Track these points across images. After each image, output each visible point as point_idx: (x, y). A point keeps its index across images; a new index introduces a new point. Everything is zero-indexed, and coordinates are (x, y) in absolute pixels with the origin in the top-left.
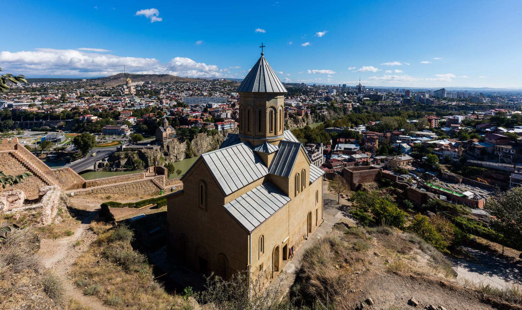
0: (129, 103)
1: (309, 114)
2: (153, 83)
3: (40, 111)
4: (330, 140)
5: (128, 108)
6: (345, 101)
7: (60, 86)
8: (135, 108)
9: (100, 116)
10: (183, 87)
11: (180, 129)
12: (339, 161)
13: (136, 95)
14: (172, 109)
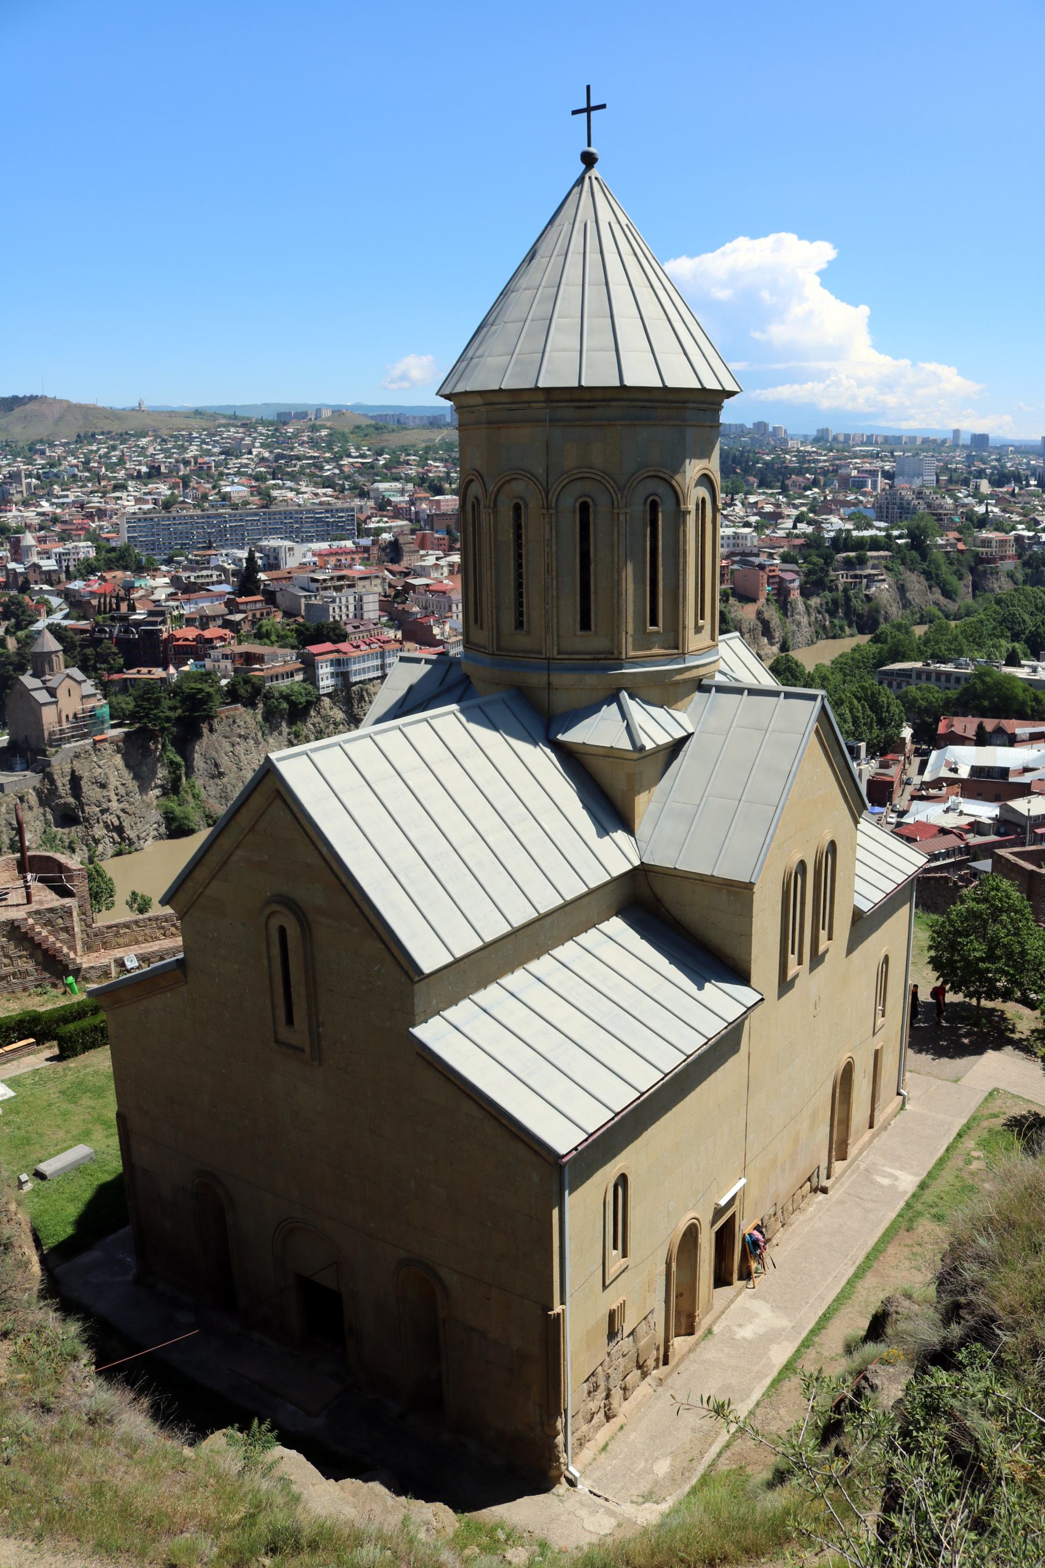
1: (795, 595)
4: (899, 726)
6: (982, 522)
10: (121, 461)
11: (125, 686)
12: (944, 831)
14: (77, 585)
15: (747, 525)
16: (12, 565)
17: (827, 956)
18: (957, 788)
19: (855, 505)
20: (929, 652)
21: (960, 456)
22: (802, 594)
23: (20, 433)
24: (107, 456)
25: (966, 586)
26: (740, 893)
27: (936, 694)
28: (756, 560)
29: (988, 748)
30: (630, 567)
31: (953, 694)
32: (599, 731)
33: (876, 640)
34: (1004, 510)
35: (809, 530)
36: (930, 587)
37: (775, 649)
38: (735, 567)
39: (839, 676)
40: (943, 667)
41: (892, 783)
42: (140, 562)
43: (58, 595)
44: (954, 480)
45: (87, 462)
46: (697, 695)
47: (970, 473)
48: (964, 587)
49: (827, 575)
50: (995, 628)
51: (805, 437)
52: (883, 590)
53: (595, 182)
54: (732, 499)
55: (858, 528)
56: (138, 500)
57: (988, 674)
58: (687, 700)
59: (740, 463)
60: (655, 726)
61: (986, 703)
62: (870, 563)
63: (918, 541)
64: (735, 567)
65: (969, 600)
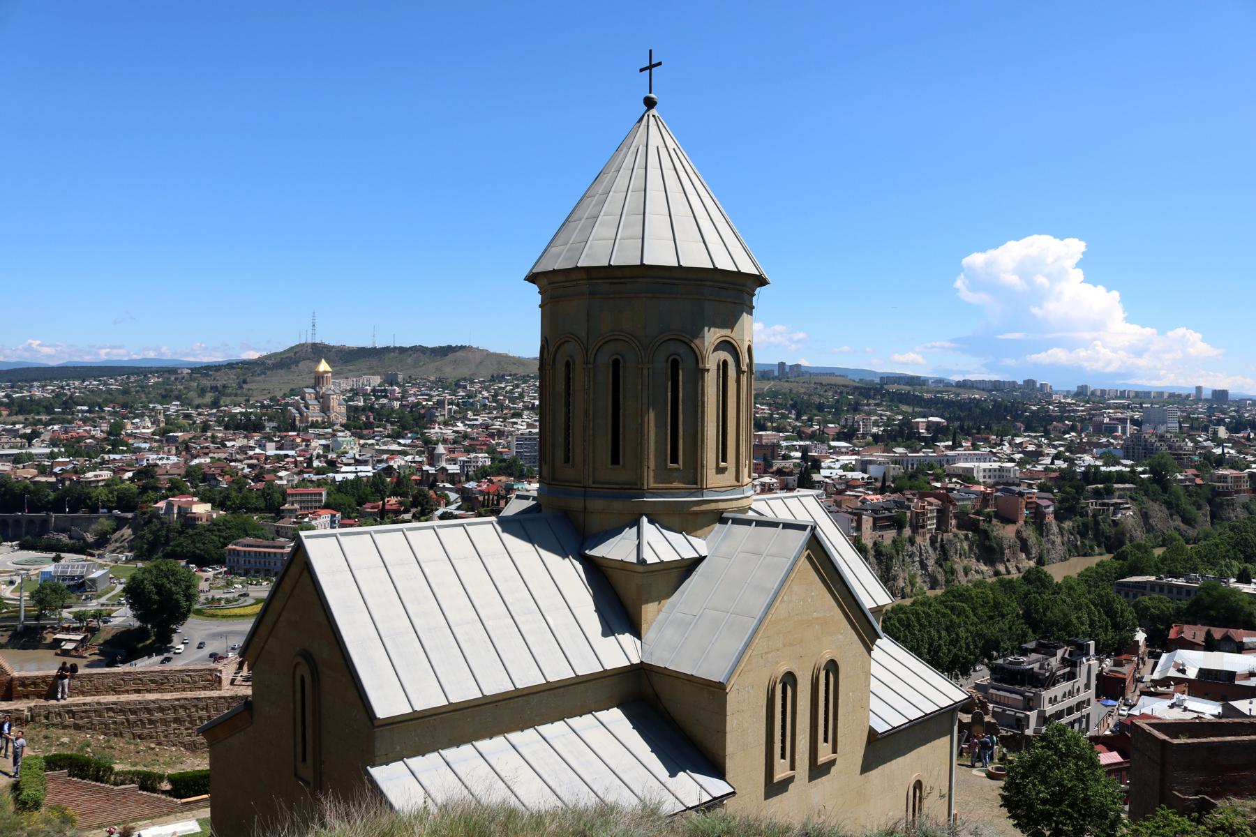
0: (318, 456)
1: (1050, 518)
2: (410, 379)
3: (43, 479)
4: (1133, 630)
5: (315, 478)
6: (1220, 461)
7: (109, 392)
8: (339, 477)
9: (219, 502)
10: (521, 396)
13: (346, 427)
14: (472, 485)
15: (1012, 460)
16: (426, 468)
17: (833, 769)
18: (1183, 687)
19: (1106, 446)
20: (1166, 569)
21: (1201, 408)
22: (1056, 518)
23: (450, 372)
24: (511, 392)
25: (1205, 515)
26: (715, 692)
27: (1168, 605)
28: (1017, 489)
29: (1215, 653)
30: (652, 415)
31: (1184, 604)
32: (617, 549)
33: (1117, 558)
34: (1239, 452)
35: (1064, 465)
36: (1171, 515)
37: (1032, 563)
38: (999, 494)
39: (1084, 588)
40: (1174, 581)
41: (1124, 680)
42: (522, 471)
43: (457, 492)
44: (1194, 426)
45: (495, 396)
46: (718, 526)
47: (1211, 421)
48: (1203, 516)
49: (1078, 503)
50: (1228, 551)
51: (1068, 392)
52: (1128, 515)
53: (652, 119)
54: (1002, 440)
55: (1105, 465)
56: (529, 426)
57: (1215, 588)
58: (706, 529)
59: (1010, 412)
60: (660, 545)
61: (1212, 613)
62: (1117, 494)
63: (1159, 476)
64: (999, 494)
65: (1207, 527)
